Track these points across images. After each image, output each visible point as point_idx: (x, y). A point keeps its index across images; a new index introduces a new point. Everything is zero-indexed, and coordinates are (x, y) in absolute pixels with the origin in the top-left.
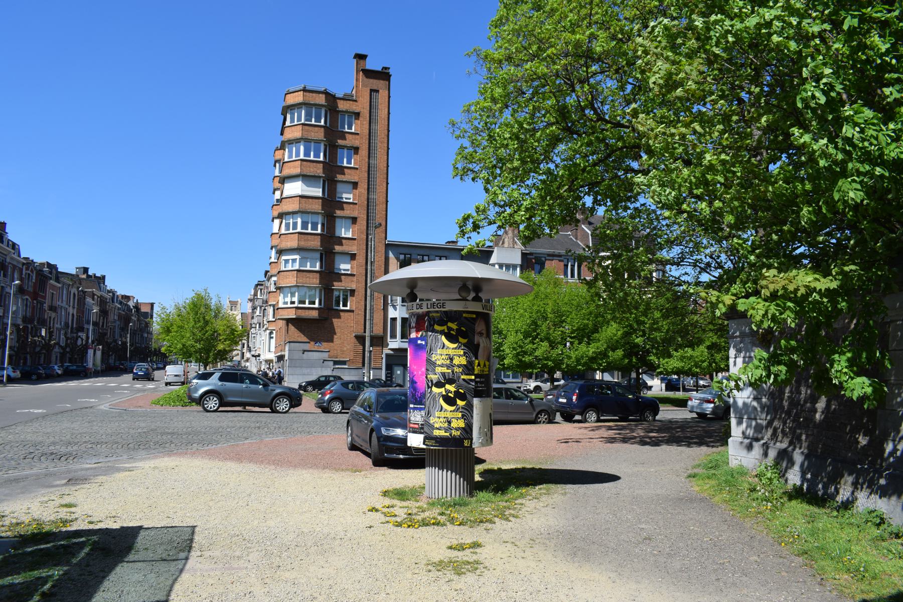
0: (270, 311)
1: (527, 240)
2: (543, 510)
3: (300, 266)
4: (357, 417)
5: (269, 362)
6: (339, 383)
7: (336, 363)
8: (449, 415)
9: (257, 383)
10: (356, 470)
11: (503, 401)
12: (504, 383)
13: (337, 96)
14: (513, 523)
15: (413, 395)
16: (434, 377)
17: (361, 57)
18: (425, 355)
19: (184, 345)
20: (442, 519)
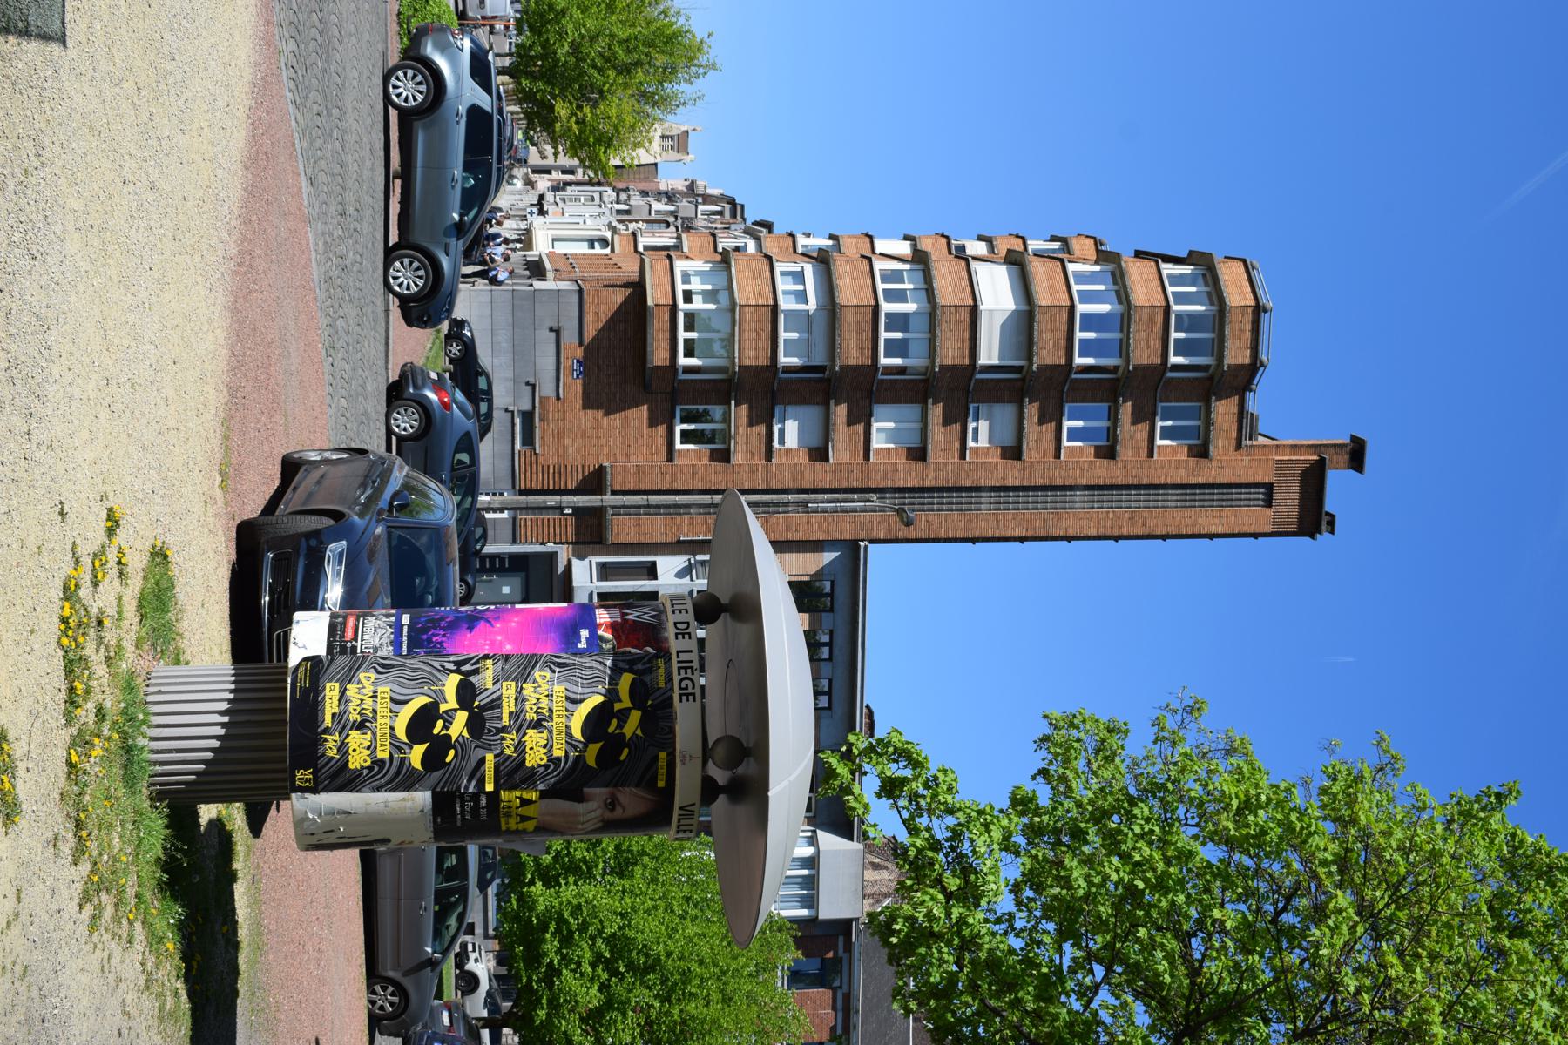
0: (666, 239)
1: (881, 927)
2: (114, 1003)
3: (788, 313)
4: (376, 475)
5: (526, 239)
6: (470, 425)
7: (528, 417)
8: (382, 723)
9: (465, 208)
10: (228, 476)
11: (431, 882)
12: (483, 885)
13: (1250, 396)
14: (75, 918)
15: (435, 623)
16: (486, 679)
17: (1356, 455)
18: (547, 650)
19: (563, 13)
20: (86, 714)
